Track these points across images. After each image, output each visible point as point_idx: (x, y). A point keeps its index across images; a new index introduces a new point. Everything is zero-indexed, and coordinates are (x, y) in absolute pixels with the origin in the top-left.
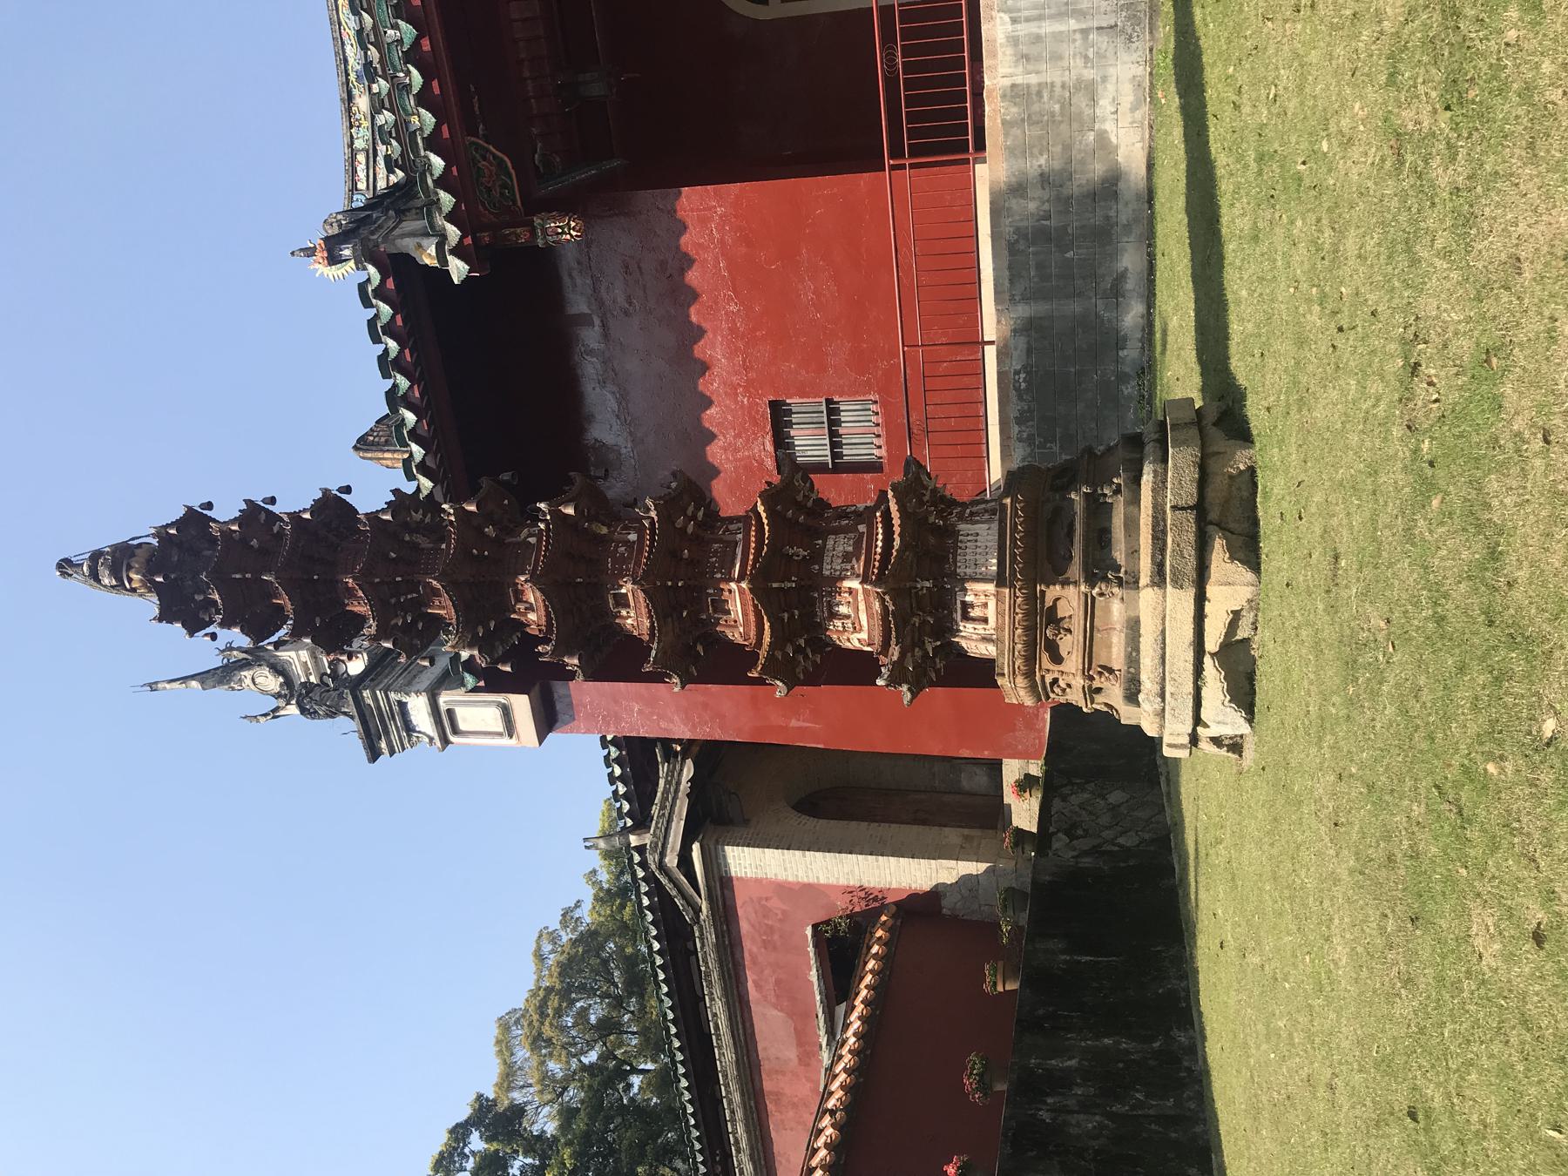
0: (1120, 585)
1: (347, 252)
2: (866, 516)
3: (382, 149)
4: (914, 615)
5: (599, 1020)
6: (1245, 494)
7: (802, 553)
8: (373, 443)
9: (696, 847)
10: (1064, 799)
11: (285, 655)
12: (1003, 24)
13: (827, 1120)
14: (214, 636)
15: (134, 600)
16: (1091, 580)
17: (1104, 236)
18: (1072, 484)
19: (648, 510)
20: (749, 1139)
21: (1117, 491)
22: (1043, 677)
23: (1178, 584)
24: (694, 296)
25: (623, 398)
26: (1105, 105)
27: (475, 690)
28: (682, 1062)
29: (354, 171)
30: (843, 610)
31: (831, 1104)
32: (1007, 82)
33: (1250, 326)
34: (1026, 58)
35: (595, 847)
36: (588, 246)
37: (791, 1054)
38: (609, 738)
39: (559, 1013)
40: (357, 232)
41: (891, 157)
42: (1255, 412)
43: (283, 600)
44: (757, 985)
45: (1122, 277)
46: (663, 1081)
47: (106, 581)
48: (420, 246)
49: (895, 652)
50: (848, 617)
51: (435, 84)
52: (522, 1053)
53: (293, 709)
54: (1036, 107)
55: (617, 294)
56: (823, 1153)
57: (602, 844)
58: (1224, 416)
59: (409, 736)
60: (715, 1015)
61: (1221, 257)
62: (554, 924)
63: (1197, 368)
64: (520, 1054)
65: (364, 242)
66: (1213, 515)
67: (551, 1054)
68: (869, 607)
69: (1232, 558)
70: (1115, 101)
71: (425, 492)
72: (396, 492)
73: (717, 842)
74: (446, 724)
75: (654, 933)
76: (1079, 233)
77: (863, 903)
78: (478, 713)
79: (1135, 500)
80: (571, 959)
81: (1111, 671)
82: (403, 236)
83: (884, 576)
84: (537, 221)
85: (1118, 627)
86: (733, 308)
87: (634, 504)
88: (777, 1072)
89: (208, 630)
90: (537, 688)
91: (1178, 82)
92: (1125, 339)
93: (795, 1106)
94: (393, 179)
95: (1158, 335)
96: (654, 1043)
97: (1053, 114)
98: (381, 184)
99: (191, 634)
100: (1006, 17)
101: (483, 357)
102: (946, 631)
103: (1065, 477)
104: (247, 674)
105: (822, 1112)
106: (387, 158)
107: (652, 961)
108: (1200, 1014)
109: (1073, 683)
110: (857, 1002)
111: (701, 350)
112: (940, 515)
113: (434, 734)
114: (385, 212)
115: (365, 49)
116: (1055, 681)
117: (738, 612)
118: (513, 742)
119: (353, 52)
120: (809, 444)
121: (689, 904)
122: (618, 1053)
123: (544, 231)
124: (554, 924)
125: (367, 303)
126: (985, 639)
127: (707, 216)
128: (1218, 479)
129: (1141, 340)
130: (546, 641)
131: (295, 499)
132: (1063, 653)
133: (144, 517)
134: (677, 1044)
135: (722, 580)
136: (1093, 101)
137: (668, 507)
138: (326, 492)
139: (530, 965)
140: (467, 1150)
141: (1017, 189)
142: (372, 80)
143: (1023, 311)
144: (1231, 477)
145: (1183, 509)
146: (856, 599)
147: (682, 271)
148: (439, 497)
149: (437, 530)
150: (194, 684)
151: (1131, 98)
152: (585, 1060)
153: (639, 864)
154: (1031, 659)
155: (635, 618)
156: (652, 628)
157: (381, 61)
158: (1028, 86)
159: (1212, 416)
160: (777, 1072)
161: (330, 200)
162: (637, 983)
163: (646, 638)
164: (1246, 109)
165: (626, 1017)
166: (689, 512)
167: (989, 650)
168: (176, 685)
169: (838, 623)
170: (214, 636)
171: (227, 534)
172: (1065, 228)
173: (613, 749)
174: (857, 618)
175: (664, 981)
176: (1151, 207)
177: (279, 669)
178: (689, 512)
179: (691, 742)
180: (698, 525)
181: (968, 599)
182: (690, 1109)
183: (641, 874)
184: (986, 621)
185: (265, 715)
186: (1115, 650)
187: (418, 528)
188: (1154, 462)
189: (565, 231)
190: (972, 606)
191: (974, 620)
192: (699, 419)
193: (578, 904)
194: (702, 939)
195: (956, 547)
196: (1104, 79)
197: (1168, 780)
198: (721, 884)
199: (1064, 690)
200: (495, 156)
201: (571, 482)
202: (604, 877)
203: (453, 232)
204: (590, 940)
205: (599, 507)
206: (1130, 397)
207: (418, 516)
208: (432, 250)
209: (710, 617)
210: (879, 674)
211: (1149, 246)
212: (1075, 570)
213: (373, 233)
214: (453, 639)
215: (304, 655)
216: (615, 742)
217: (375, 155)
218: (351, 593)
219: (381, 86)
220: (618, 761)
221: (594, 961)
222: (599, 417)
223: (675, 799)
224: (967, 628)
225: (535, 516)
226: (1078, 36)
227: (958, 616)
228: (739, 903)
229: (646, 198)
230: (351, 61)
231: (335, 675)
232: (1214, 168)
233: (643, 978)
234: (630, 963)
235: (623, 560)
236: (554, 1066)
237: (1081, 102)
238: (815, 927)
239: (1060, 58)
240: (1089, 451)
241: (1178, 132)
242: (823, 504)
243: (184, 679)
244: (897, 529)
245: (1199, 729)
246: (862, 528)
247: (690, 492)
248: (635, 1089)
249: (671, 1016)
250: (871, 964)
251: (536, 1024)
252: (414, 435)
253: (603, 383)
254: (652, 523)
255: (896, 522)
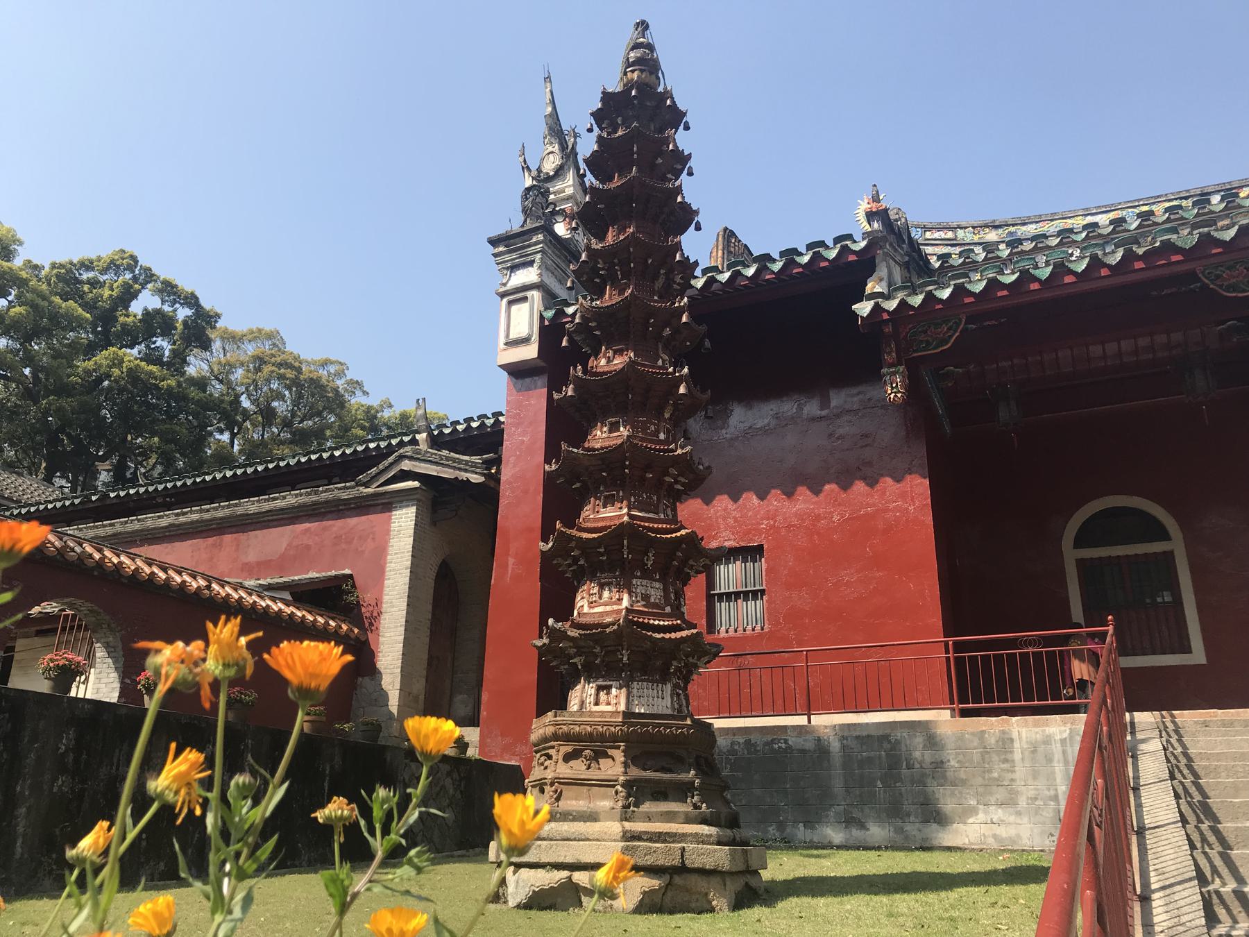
0: (624, 807)
1: (876, 225)
2: (677, 612)
3: (958, 250)
4: (602, 648)
5: (274, 409)
6: (693, 905)
7: (650, 563)
8: (729, 242)
9: (416, 484)
10: (449, 774)
11: (570, 177)
12: (1061, 732)
13: (203, 583)
14: (590, 130)
15: (619, 74)
16: (628, 785)
17: (894, 812)
18: (701, 772)
19: (682, 448)
20: (186, 523)
21: (696, 807)
22: (553, 747)
23: (625, 850)
24: (845, 487)
25: (765, 431)
26: (998, 814)
27: (542, 318)
28: (245, 472)
29: (939, 229)
30: (606, 594)
31: (214, 586)
32: (1015, 735)
33: (823, 911)
34: (1034, 751)
35: (418, 407)
36: (882, 407)
37: (252, 557)
38: (502, 419)
39: (281, 377)
40: (892, 234)
41: (955, 643)
42: (757, 912)
43: (617, 182)
44: (307, 530)
45: (862, 826)
46: (224, 459)
47: (632, 55)
48: (881, 280)
49: (574, 633)
50: (600, 598)
51: (1005, 293)
52: (250, 349)
53: (529, 182)
54: (995, 758)
55: (845, 428)
56: (178, 579)
57: (421, 412)
58: (751, 893)
59: (507, 268)
60: (284, 498)
61: (876, 894)
62: (350, 375)
63: (790, 878)
64: (250, 347)
65: (884, 239)
66: (678, 880)
67: (248, 371)
68: (608, 613)
69: (644, 893)
70: (1001, 822)
71: (693, 282)
72: (696, 263)
73: (419, 500)
74: (516, 296)
75: (348, 452)
76: (897, 791)
77: (368, 615)
78: (524, 319)
79: (689, 820)
80: (322, 388)
81: (558, 799)
82: (889, 268)
83: (632, 626)
84: (901, 368)
85: (592, 805)
86: (836, 518)
87: (687, 438)
88: (238, 545)
89: (595, 127)
90: (543, 364)
91: (1015, 868)
92: (813, 828)
93: (211, 559)
94: (933, 259)
95: (815, 852)
96: (254, 451)
97: (990, 771)
98: (929, 250)
99: (592, 114)
100: (1065, 735)
101: (794, 329)
102: (590, 672)
103: (707, 766)
104: (556, 148)
105: (209, 579)
106: (949, 255)
107: (322, 452)
108: (284, 874)
109: (548, 771)
110: (292, 608)
111: (803, 492)
112: (678, 669)
113: (509, 286)
114: (907, 254)
115: (1033, 239)
116: (549, 757)
117: (605, 514)
118: (502, 346)
119: (1031, 229)
120: (729, 576)
121: (372, 478)
122: (248, 424)
123: (894, 374)
124: (350, 375)
125: (837, 240)
126: (582, 703)
127: (907, 499)
128: (705, 884)
129: (811, 841)
130: (585, 371)
131: (692, 190)
132: (572, 763)
133: (678, 81)
134: (260, 468)
135: (629, 501)
136: (1001, 805)
137: (685, 463)
138: (696, 212)
139: (319, 356)
140: (177, 305)
141: (933, 741)
142: (1009, 244)
143: (835, 746)
144: (706, 894)
145: (682, 856)
146: (614, 604)
147: (864, 479)
148: (689, 292)
149: (668, 293)
150: (550, 109)
151: (1004, 835)
152: (243, 398)
153: (402, 441)
154: (567, 738)
155: (601, 437)
156: (594, 450)
157: (1023, 252)
158: (1012, 752)
159: (753, 882)
160: (238, 545)
161: (915, 211)
162: (301, 439)
163: (586, 445)
164: (991, 911)
165: (275, 430)
166: (681, 479)
167: (573, 705)
168: (548, 96)
169: (596, 590)
170: (590, 130)
171: (666, 141)
172: (900, 780)
173: (492, 421)
174: (599, 604)
175: (310, 459)
176: (917, 849)
177: (559, 172)
178: (681, 479)
179: (498, 481)
180: (671, 485)
181: (614, 690)
182: (208, 478)
183: (394, 442)
184: (596, 703)
185: (525, 161)
186: (574, 802)
187: (669, 281)
188: (719, 836)
189: (894, 389)
190: (608, 693)
191: (597, 695)
192: (749, 490)
193: (365, 393)
194: (345, 488)
195: (653, 682)
196: (1019, 814)
197: (463, 856)
198: (386, 504)
199: (542, 764)
200: (951, 337)
201: (703, 391)
202: (386, 414)
203: (892, 305)
204: (337, 402)
205: (685, 410)
206: (766, 832)
207: (678, 280)
208: (878, 289)
209: (602, 492)
210: (557, 621)
211: (887, 848)
212: (635, 772)
213: (891, 245)
214: (586, 303)
215: (570, 191)
216: (497, 422)
217: (952, 245)
218: (622, 230)
219: (1004, 252)
220: (483, 425)
221: (320, 405)
222: (750, 413)
223: (454, 468)
224: (591, 689)
225: (677, 364)
226: (1052, 793)
227: (601, 683)
228: (370, 517)
229: (921, 451)
230: (1024, 228)
231: (554, 213)
232: (946, 890)
233: (306, 444)
234: (319, 434)
235: (645, 429)
236: (239, 374)
237: (1000, 794)
238: (351, 576)
239: (1035, 778)
240: (726, 787)
241: (976, 868)
242: (686, 580)
243: (553, 102)
244: (667, 636)
245: (512, 868)
246: (668, 609)
247: (693, 480)
248: (218, 436)
249: (282, 464)
250: (321, 620)
251: (273, 360)
252: (737, 274)
253: (776, 416)
254: (673, 451)
255: (673, 635)
